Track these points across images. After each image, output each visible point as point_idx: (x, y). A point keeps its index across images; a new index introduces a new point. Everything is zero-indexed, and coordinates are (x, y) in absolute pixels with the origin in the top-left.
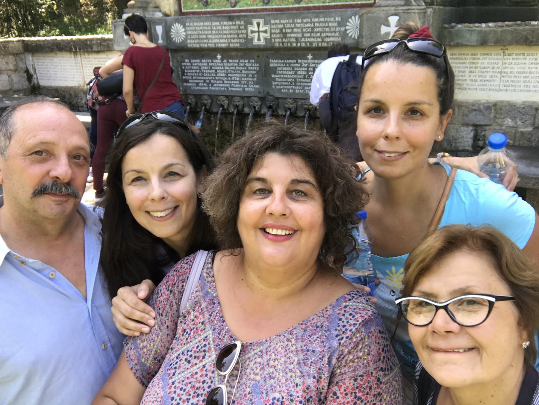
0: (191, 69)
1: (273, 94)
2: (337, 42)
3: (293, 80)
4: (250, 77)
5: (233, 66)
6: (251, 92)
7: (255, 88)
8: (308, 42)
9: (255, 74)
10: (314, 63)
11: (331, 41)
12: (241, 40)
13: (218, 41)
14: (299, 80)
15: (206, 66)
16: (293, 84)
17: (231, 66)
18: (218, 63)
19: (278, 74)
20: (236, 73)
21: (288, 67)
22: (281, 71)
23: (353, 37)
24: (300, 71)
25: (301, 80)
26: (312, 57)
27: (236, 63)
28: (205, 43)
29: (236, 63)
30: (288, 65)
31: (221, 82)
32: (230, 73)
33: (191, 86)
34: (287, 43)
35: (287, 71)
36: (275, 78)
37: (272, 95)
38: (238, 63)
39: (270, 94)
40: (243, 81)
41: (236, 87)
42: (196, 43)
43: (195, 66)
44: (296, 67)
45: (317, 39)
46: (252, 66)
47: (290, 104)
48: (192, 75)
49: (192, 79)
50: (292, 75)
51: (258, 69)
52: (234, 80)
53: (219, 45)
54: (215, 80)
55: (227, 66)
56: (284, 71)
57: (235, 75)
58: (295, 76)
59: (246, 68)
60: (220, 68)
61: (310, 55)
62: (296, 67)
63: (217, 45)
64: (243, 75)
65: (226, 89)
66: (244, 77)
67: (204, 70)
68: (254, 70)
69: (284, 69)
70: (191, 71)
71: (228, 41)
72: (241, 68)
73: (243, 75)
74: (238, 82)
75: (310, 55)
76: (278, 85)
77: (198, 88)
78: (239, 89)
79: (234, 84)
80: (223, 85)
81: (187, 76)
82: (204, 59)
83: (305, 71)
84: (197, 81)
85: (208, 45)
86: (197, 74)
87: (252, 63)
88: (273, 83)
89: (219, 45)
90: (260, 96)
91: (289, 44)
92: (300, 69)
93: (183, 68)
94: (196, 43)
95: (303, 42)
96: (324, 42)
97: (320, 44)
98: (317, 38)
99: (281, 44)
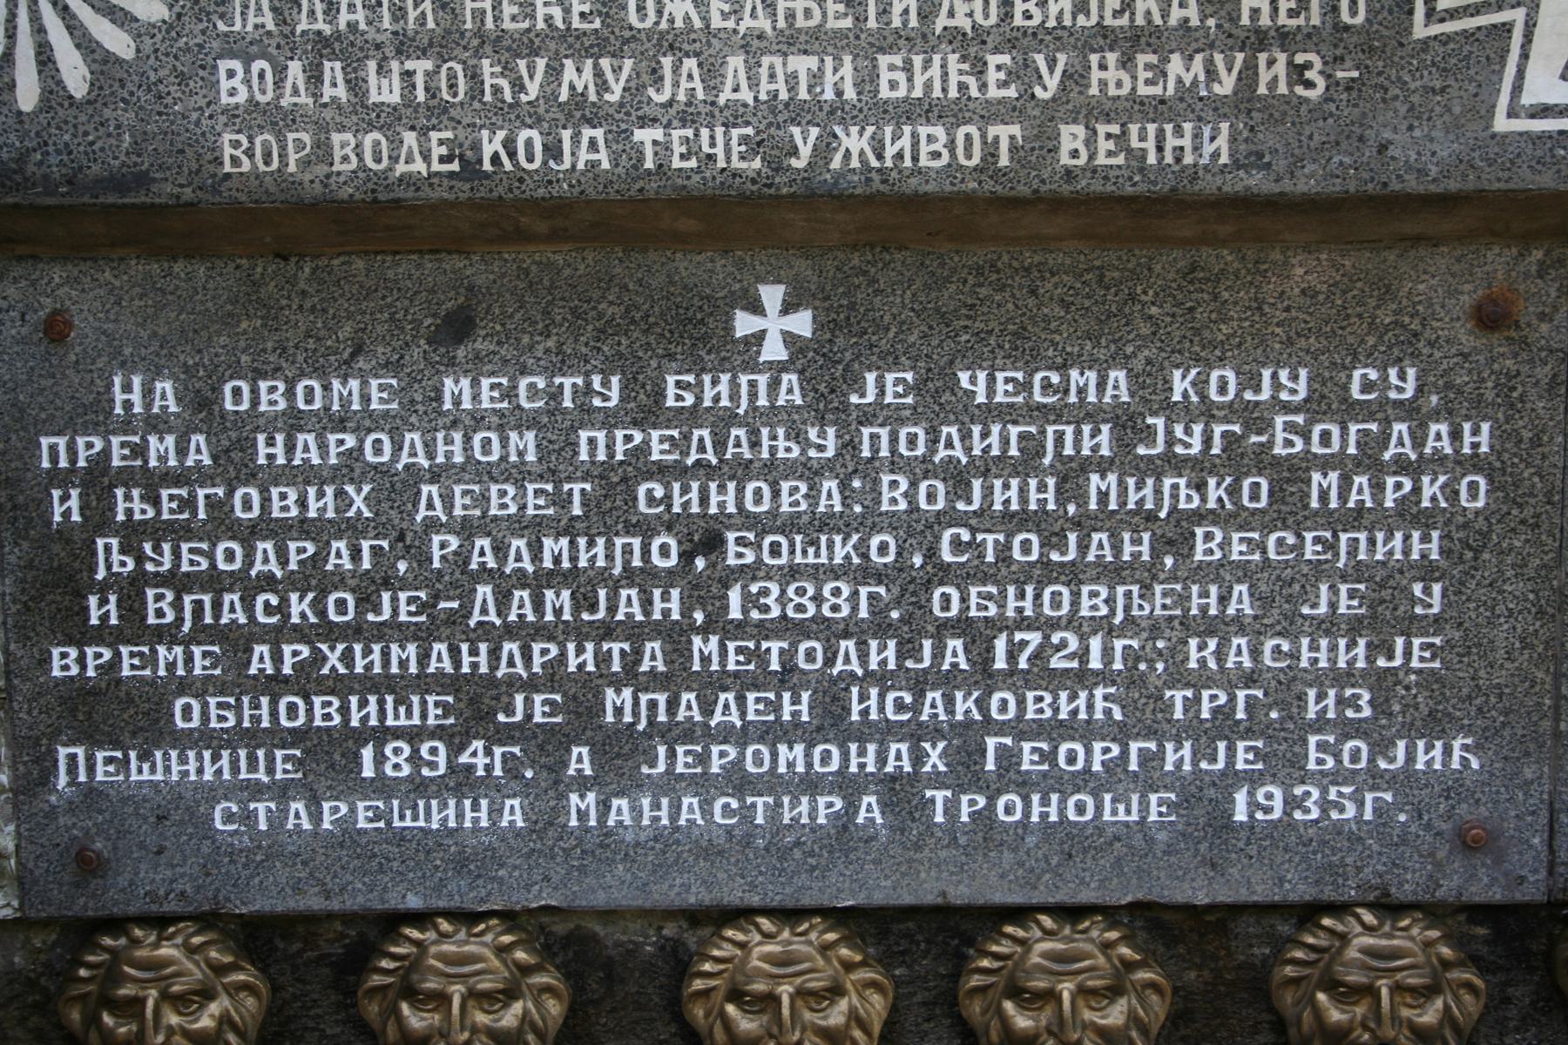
0: (222, 522)
4: (1328, 626)
5: (1028, 462)
6: (1329, 834)
7: (1405, 780)
9: (1427, 572)
12: (1273, 72)
13: (841, 78)
15: (518, 474)
17: (987, 467)
18: (755, 420)
20: (1073, 575)
26: (802, 323)
27: (1091, 415)
28: (581, 111)
29: (1091, 415)
31: (798, 707)
32: (963, 577)
33: (213, 793)
38: (1128, 425)
40: (1200, 680)
41: (1056, 783)
42: (389, 120)
43: (306, 476)
46: (1369, 459)
47: (475, 997)
48: (233, 611)
49: (237, 683)
51: (1476, 495)
52: (1041, 675)
53: (854, 141)
54: (672, 681)
55: (922, 469)
57: (1055, 598)
59: (1257, 490)
60: (792, 497)
63: (805, 141)
64: (1203, 600)
65: (870, 808)
66: (1216, 627)
68: (1410, 514)
70: (227, 555)
71: (1022, 73)
72: (1178, 492)
73: (1203, 600)
74: (1100, 703)
77: (332, 812)
78: (1117, 813)
79: (1020, 729)
80: (829, 759)
81: (134, 627)
82: (476, 368)
84: (324, 711)
85: (618, 137)
86: (341, 607)
87: (1384, 411)
89: (854, 141)
90: (1485, 888)
93: (67, 507)
94: (389, 120)
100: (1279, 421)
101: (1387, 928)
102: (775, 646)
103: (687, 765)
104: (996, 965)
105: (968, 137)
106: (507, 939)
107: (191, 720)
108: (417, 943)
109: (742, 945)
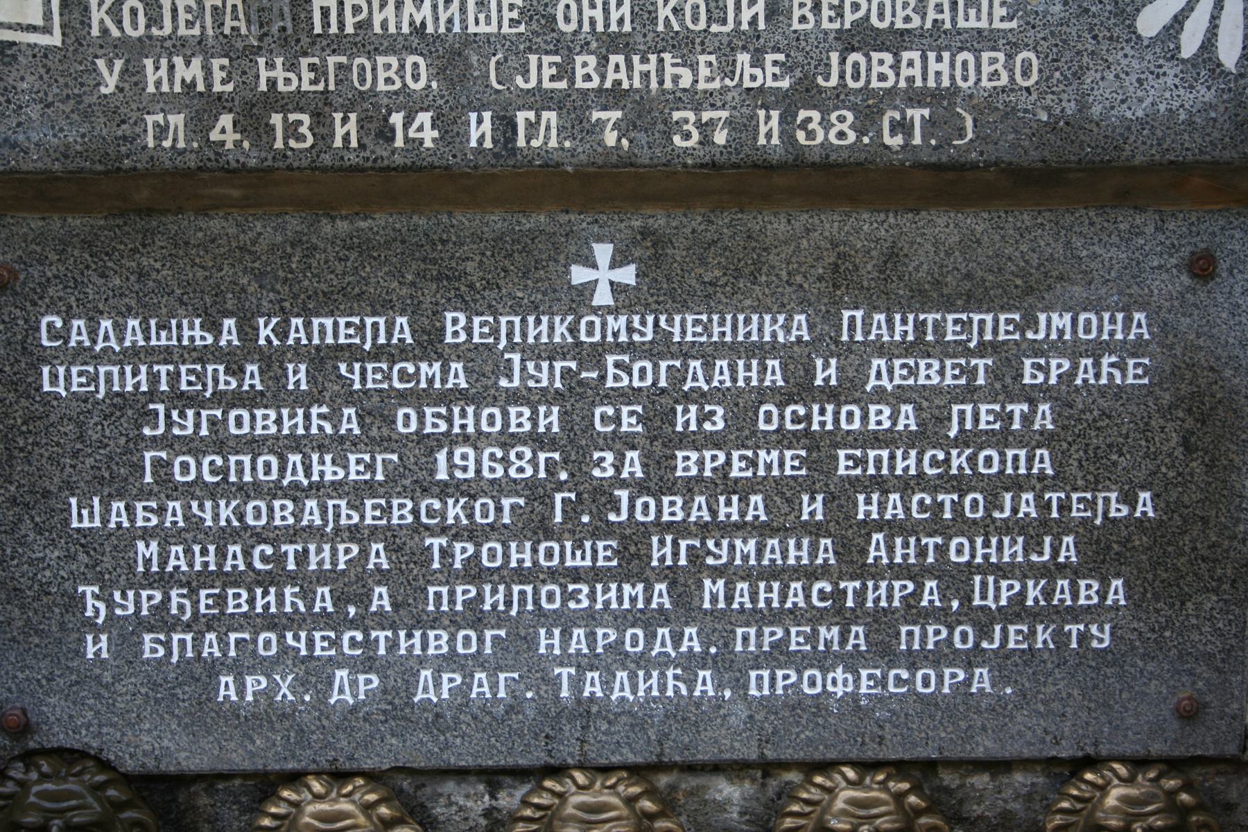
1: (85, 739)
2: (983, 106)
3: (379, 558)
8: (614, 96)
10: (660, 348)
11: (915, 97)
14: (462, 551)
16: (381, 598)
19: (166, 486)
21: (304, 400)
22: (194, 446)
23: (1190, 43)
24: (477, 440)
25: (491, 553)
30: (298, 376)
34: (320, 107)
35: (283, 445)
36: (128, 538)
37: (69, 756)
39: (60, 738)
44: (418, 398)
45: (727, 68)
50: (357, 493)
56: (254, 445)
58: (401, 512)
61: (603, 252)
62: (418, 398)
67: (584, 664)
69: (239, 423)
75: (603, 252)
76: (162, 620)
83: (538, 441)
88: (94, 607)
91: (346, 129)
92: (466, 419)
95: (540, 99)
96: (826, 102)
97: (769, 126)
98: (726, 51)
99: (224, 130)
100: (610, 359)
101: (334, 795)
102: (290, 549)
103: (323, 649)
104: (808, 809)
105: (965, 63)
106: (372, 797)
107: (435, 593)
108: (291, 803)
109: (560, 795)
